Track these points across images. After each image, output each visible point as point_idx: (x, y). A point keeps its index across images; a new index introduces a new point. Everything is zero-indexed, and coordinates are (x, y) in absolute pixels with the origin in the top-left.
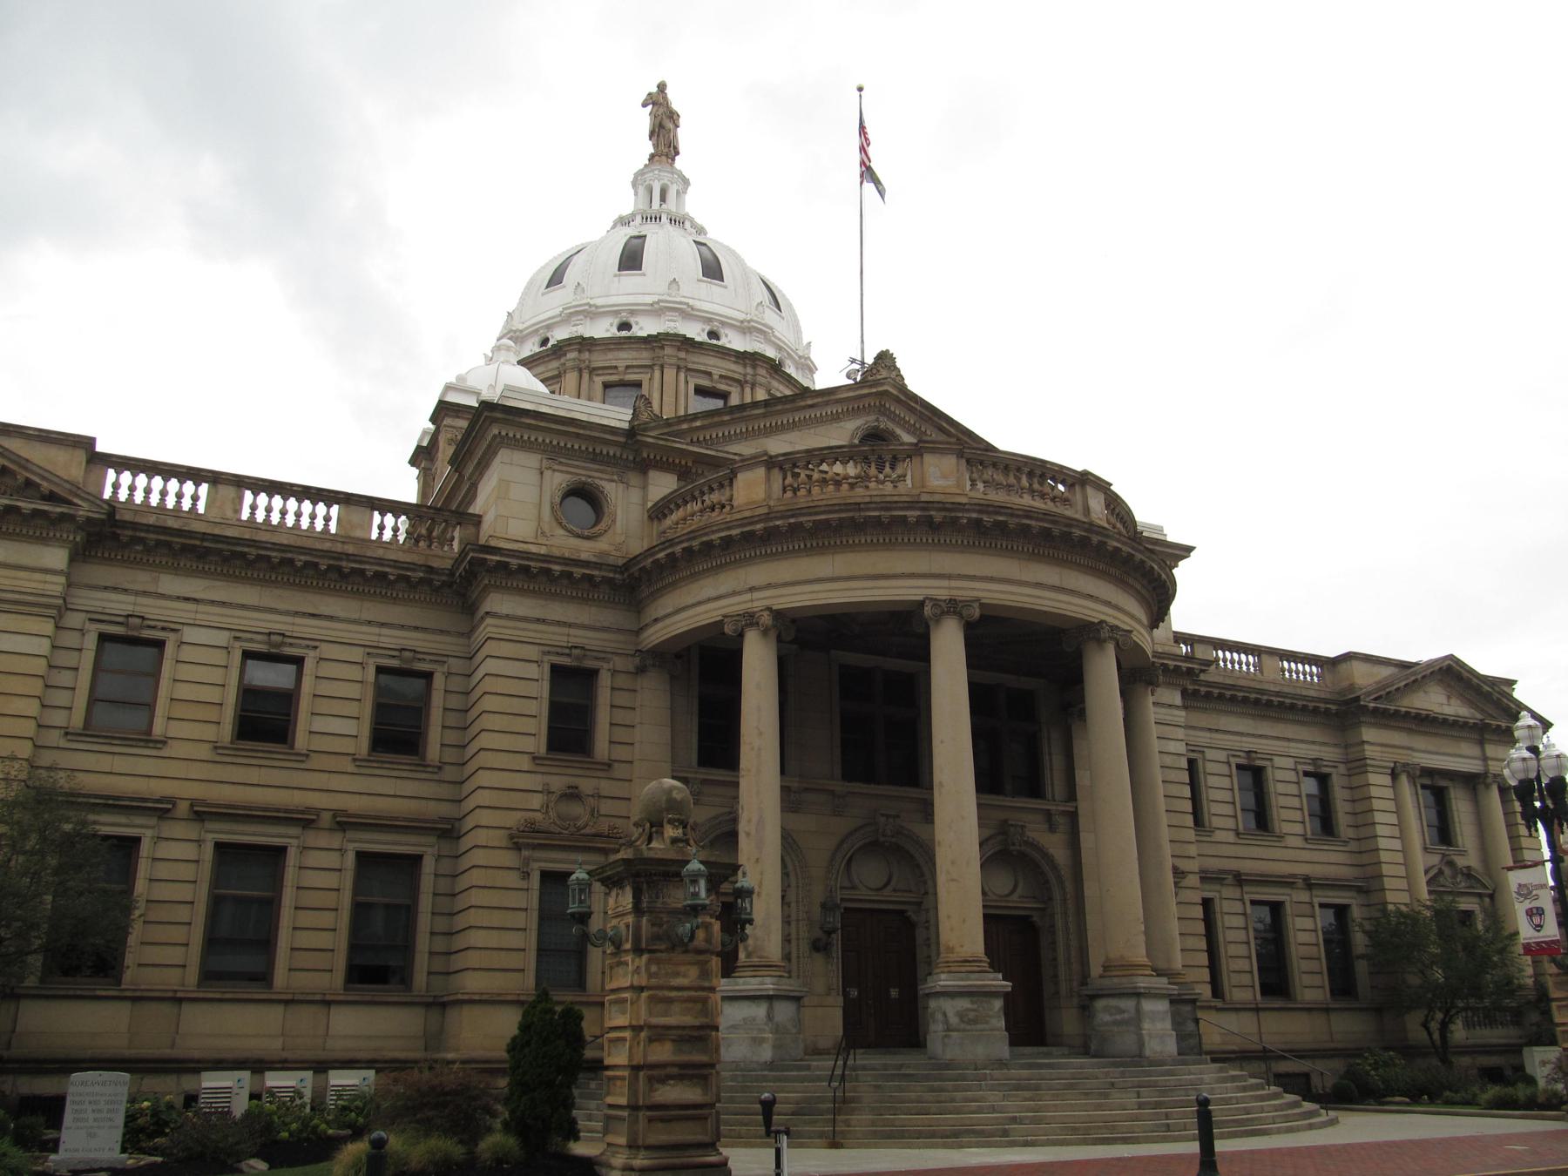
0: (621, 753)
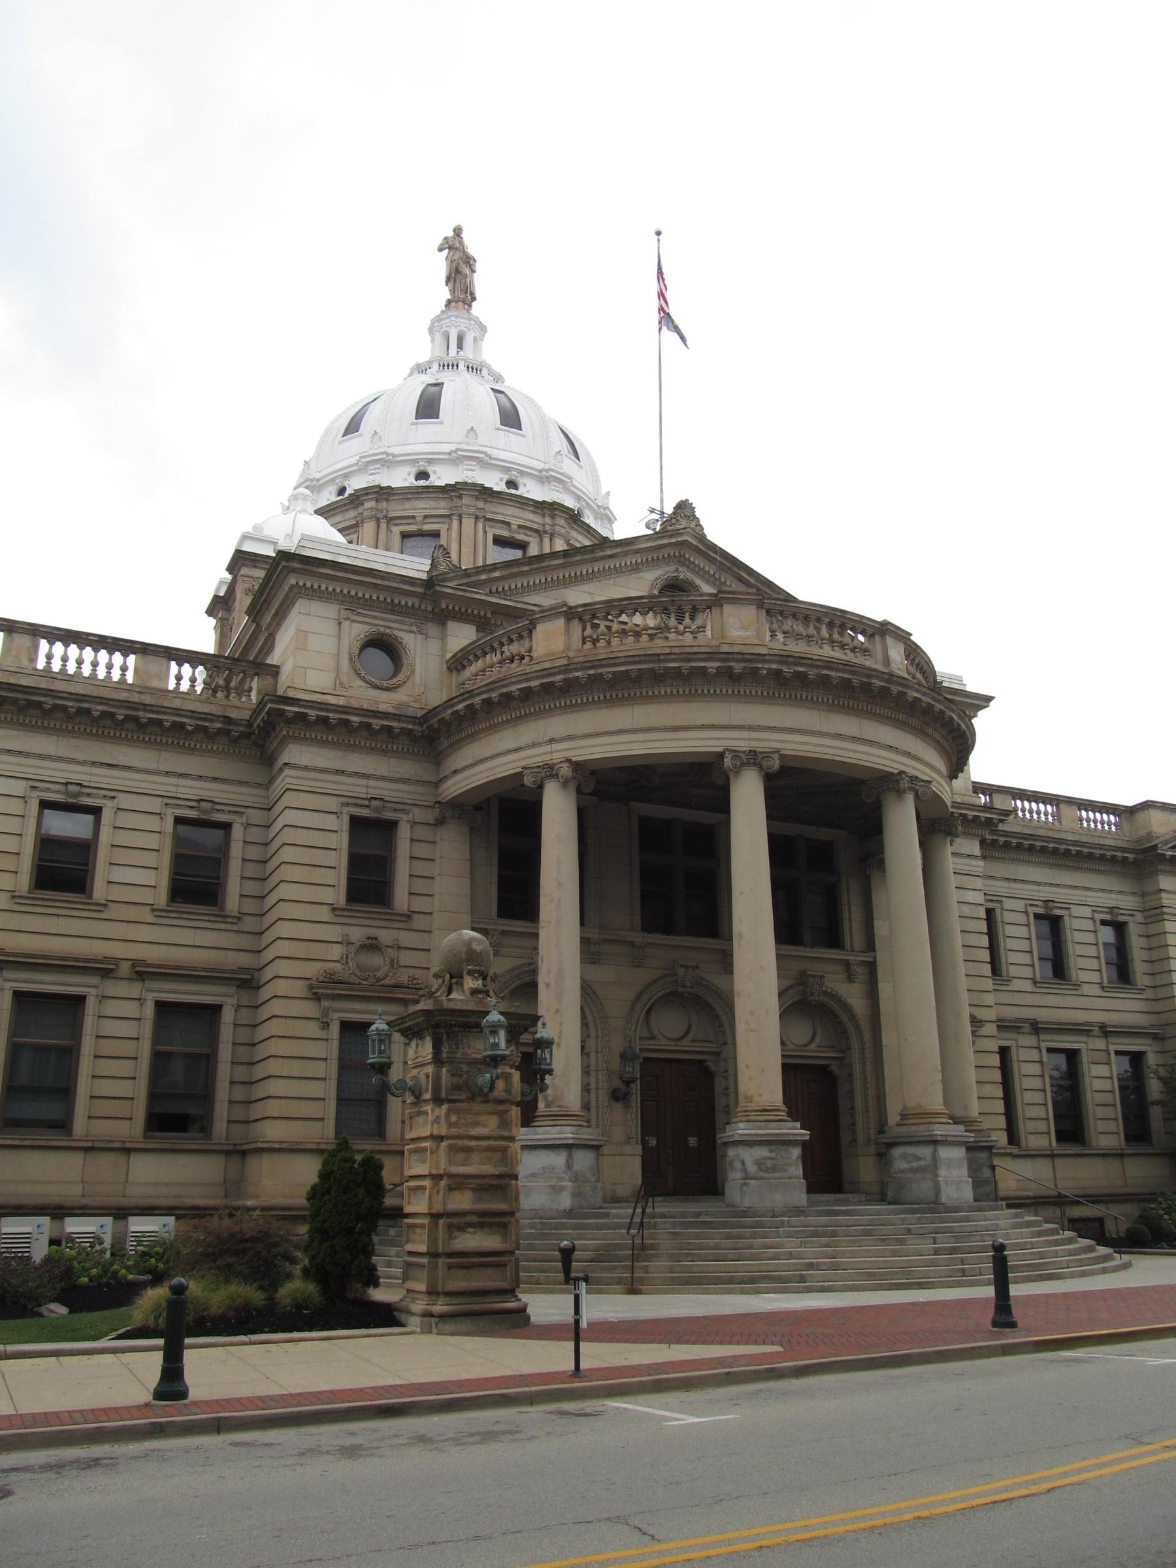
0: (419, 904)
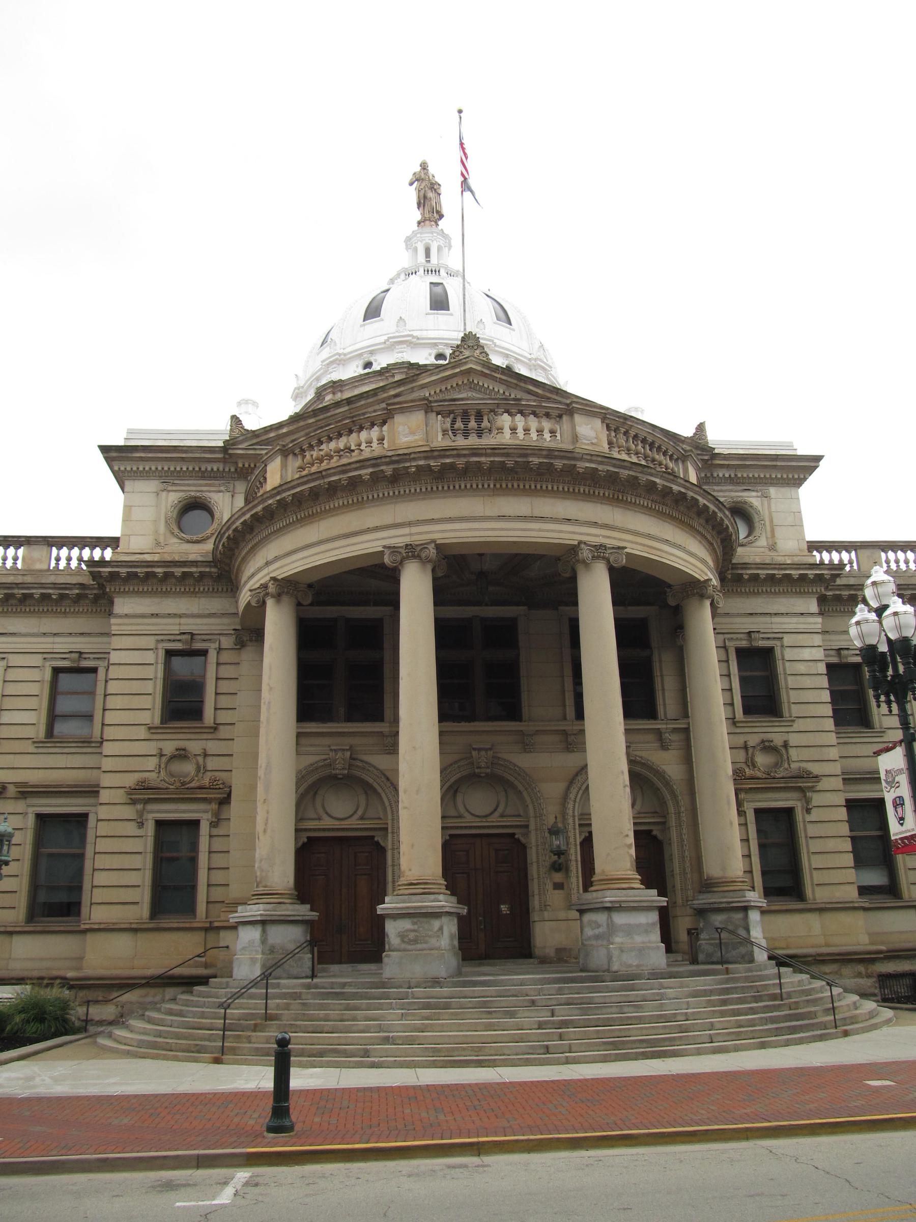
0: (223, 717)
